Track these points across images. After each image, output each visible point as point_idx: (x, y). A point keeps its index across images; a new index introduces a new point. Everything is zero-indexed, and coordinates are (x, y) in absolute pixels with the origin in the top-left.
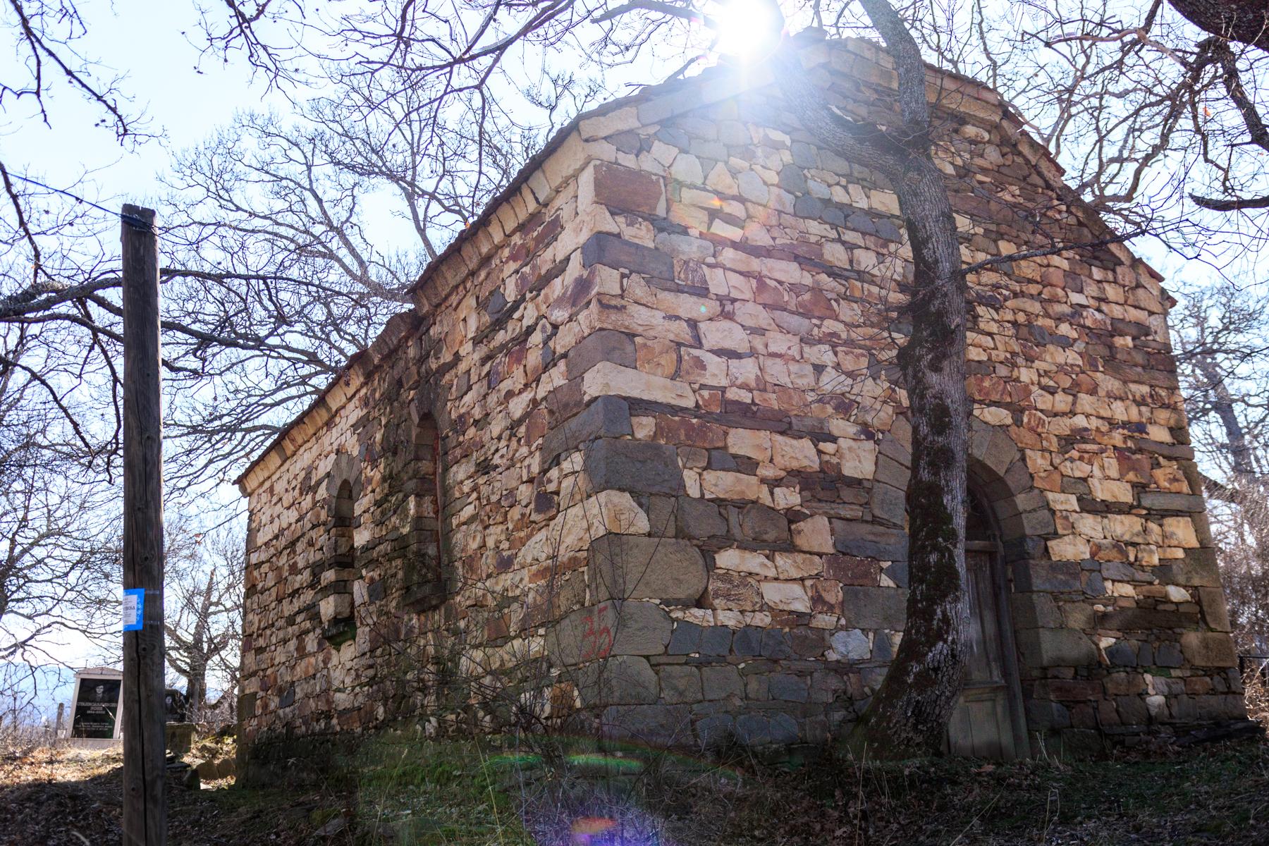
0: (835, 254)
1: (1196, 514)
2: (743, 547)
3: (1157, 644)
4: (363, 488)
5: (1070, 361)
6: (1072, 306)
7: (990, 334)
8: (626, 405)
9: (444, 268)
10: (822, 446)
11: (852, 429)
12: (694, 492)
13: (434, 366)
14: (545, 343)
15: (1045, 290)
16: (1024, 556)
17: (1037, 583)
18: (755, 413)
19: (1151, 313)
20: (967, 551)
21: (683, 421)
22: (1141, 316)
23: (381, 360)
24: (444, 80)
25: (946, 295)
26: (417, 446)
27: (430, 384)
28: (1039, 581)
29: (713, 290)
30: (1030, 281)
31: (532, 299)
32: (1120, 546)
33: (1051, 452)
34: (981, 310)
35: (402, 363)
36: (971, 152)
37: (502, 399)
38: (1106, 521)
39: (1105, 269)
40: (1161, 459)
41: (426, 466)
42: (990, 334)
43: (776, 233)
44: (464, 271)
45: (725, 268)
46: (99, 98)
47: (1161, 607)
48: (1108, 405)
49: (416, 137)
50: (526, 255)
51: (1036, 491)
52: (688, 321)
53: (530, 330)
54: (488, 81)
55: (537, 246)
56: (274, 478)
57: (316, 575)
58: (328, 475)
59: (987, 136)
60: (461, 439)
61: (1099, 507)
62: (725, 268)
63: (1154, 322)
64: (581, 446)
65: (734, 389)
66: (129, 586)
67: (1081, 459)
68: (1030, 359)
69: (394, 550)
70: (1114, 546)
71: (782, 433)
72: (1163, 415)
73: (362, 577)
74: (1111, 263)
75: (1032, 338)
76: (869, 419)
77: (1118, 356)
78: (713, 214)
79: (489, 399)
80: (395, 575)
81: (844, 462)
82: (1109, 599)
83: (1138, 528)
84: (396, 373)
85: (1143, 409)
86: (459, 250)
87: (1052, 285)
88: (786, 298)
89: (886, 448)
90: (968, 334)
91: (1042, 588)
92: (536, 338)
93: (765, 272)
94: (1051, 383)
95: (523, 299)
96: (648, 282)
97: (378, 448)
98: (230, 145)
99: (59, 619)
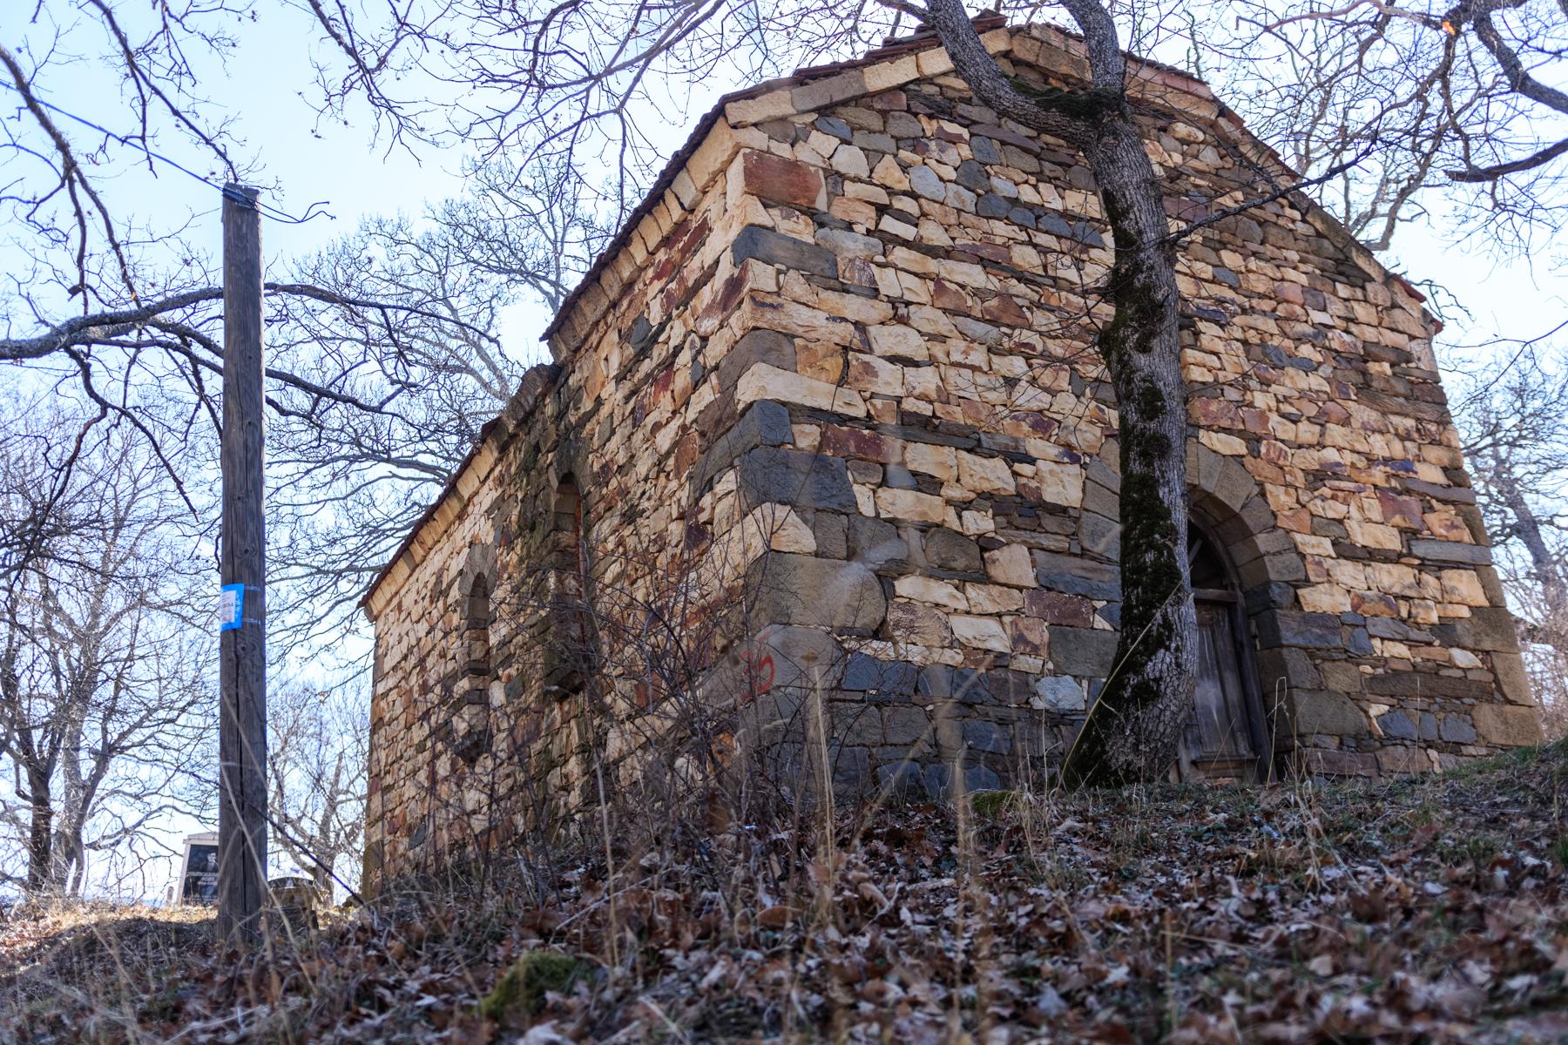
0: (1026, 258)
1: (1481, 568)
2: (931, 575)
3: (1442, 715)
4: (499, 577)
5: (1314, 387)
6: (1313, 325)
7: (1216, 354)
8: (785, 411)
9: (582, 303)
10: (1017, 467)
11: (1053, 451)
12: (867, 509)
13: (573, 420)
14: (694, 359)
15: (1280, 307)
16: (1270, 605)
17: (1287, 636)
18: (936, 427)
19: (1412, 338)
20: (1197, 601)
21: (852, 432)
22: (1401, 340)
23: (517, 426)
24: (579, 106)
25: (1152, 268)
26: (558, 515)
27: (569, 441)
28: (1289, 634)
29: (883, 291)
30: (1262, 296)
31: (679, 316)
32: (1390, 599)
33: (1296, 488)
34: (1202, 326)
35: (539, 426)
36: (1183, 154)
37: (648, 434)
38: (1369, 569)
39: (1353, 285)
40: (1434, 502)
41: (566, 538)
42: (1216, 354)
43: (955, 232)
44: (605, 303)
45: (897, 268)
46: (208, 142)
47: (1444, 672)
48: (1363, 436)
49: (560, 235)
50: (671, 270)
51: (1281, 532)
52: (856, 324)
53: (678, 350)
54: (627, 106)
55: (683, 257)
56: (403, 592)
57: (447, 690)
58: (461, 573)
59: (1201, 136)
60: (604, 491)
61: (1360, 554)
62: (897, 268)
63: (1415, 347)
64: (736, 462)
65: (912, 399)
66: (227, 582)
67: (1334, 498)
68: (1266, 383)
69: (532, 637)
70: (1381, 599)
71: (969, 451)
72: (1433, 453)
73: (498, 678)
74: (1359, 279)
75: (1267, 361)
76: (1072, 440)
77: (1374, 384)
78: (882, 210)
79: (634, 438)
80: (533, 665)
81: (1044, 486)
82: (1379, 659)
83: (1410, 580)
84: (532, 439)
85: (1408, 444)
86: (598, 279)
87: (1288, 302)
88: (970, 303)
89: (1093, 472)
90: (1189, 351)
91: (1294, 642)
92: (685, 357)
93: (943, 274)
94: (1293, 410)
95: (670, 318)
96: (808, 280)
97: (514, 527)
98: (356, 254)
99: (170, 801)
